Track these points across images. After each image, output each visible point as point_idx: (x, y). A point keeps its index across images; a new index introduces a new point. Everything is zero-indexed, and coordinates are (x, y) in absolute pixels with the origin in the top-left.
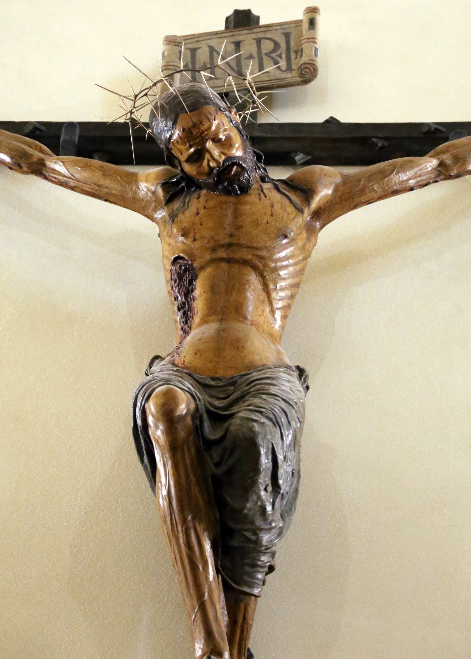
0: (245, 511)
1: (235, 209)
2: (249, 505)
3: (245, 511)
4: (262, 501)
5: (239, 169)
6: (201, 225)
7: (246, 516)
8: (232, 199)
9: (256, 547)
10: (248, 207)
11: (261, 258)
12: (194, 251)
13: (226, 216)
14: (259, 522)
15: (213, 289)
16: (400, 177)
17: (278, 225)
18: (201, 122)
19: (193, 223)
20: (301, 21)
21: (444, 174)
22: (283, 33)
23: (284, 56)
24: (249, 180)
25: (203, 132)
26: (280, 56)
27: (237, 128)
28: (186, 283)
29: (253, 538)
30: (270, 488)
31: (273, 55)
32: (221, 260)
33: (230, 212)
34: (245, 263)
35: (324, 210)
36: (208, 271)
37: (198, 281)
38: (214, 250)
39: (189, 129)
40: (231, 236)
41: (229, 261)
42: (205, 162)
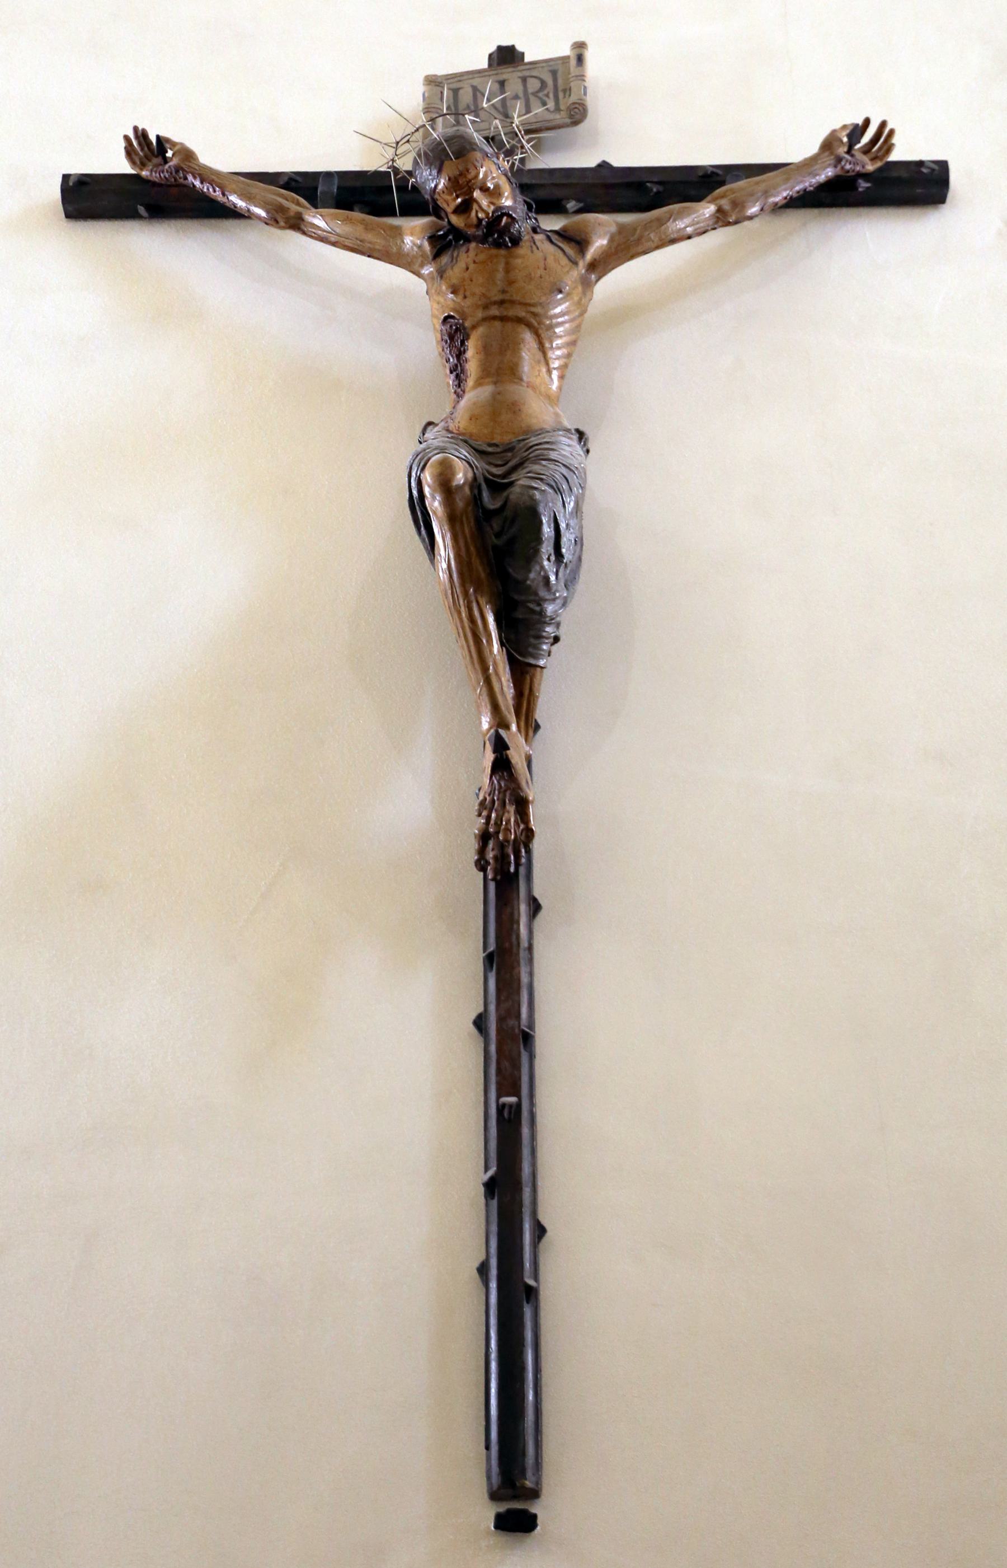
0: (528, 582)
1: (507, 263)
2: (532, 575)
3: (528, 582)
4: (546, 571)
5: (510, 220)
7: (529, 587)
9: (540, 619)
10: (519, 261)
11: (535, 315)
13: (497, 271)
14: (543, 593)
15: (486, 349)
18: (468, 171)
19: (464, 280)
20: (568, 57)
23: (551, 95)
25: (470, 181)
26: (547, 96)
27: (506, 175)
29: (537, 609)
30: (553, 558)
32: (494, 318)
33: (501, 267)
34: (519, 320)
36: (481, 330)
38: (486, 307)
40: (504, 292)
41: (503, 319)
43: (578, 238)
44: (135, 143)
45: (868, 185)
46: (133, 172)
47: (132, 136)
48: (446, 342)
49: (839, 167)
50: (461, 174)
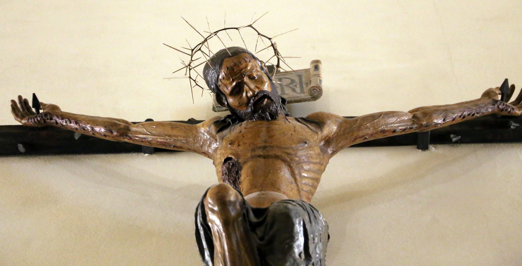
1: (268, 128)
5: (269, 101)
6: (243, 137)
8: (265, 122)
10: (277, 126)
11: (288, 154)
12: (239, 152)
13: (262, 131)
15: (253, 173)
16: (385, 121)
17: (299, 136)
18: (240, 62)
19: (238, 137)
20: (309, 69)
21: (417, 124)
22: (298, 76)
23: (298, 86)
24: (277, 110)
26: (296, 86)
27: (266, 73)
28: (234, 174)
30: (303, 255)
31: (291, 86)
32: (259, 156)
33: (264, 129)
34: (277, 157)
35: (333, 139)
36: (249, 164)
37: (242, 171)
39: (232, 67)
40: (265, 142)
41: (265, 157)
42: (244, 94)
43: (317, 121)
44: (19, 105)
45: (518, 125)
46: (17, 123)
47: (17, 101)
48: (226, 174)
49: (496, 106)
50: (235, 65)
